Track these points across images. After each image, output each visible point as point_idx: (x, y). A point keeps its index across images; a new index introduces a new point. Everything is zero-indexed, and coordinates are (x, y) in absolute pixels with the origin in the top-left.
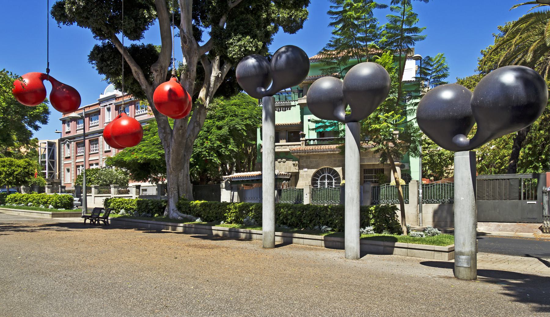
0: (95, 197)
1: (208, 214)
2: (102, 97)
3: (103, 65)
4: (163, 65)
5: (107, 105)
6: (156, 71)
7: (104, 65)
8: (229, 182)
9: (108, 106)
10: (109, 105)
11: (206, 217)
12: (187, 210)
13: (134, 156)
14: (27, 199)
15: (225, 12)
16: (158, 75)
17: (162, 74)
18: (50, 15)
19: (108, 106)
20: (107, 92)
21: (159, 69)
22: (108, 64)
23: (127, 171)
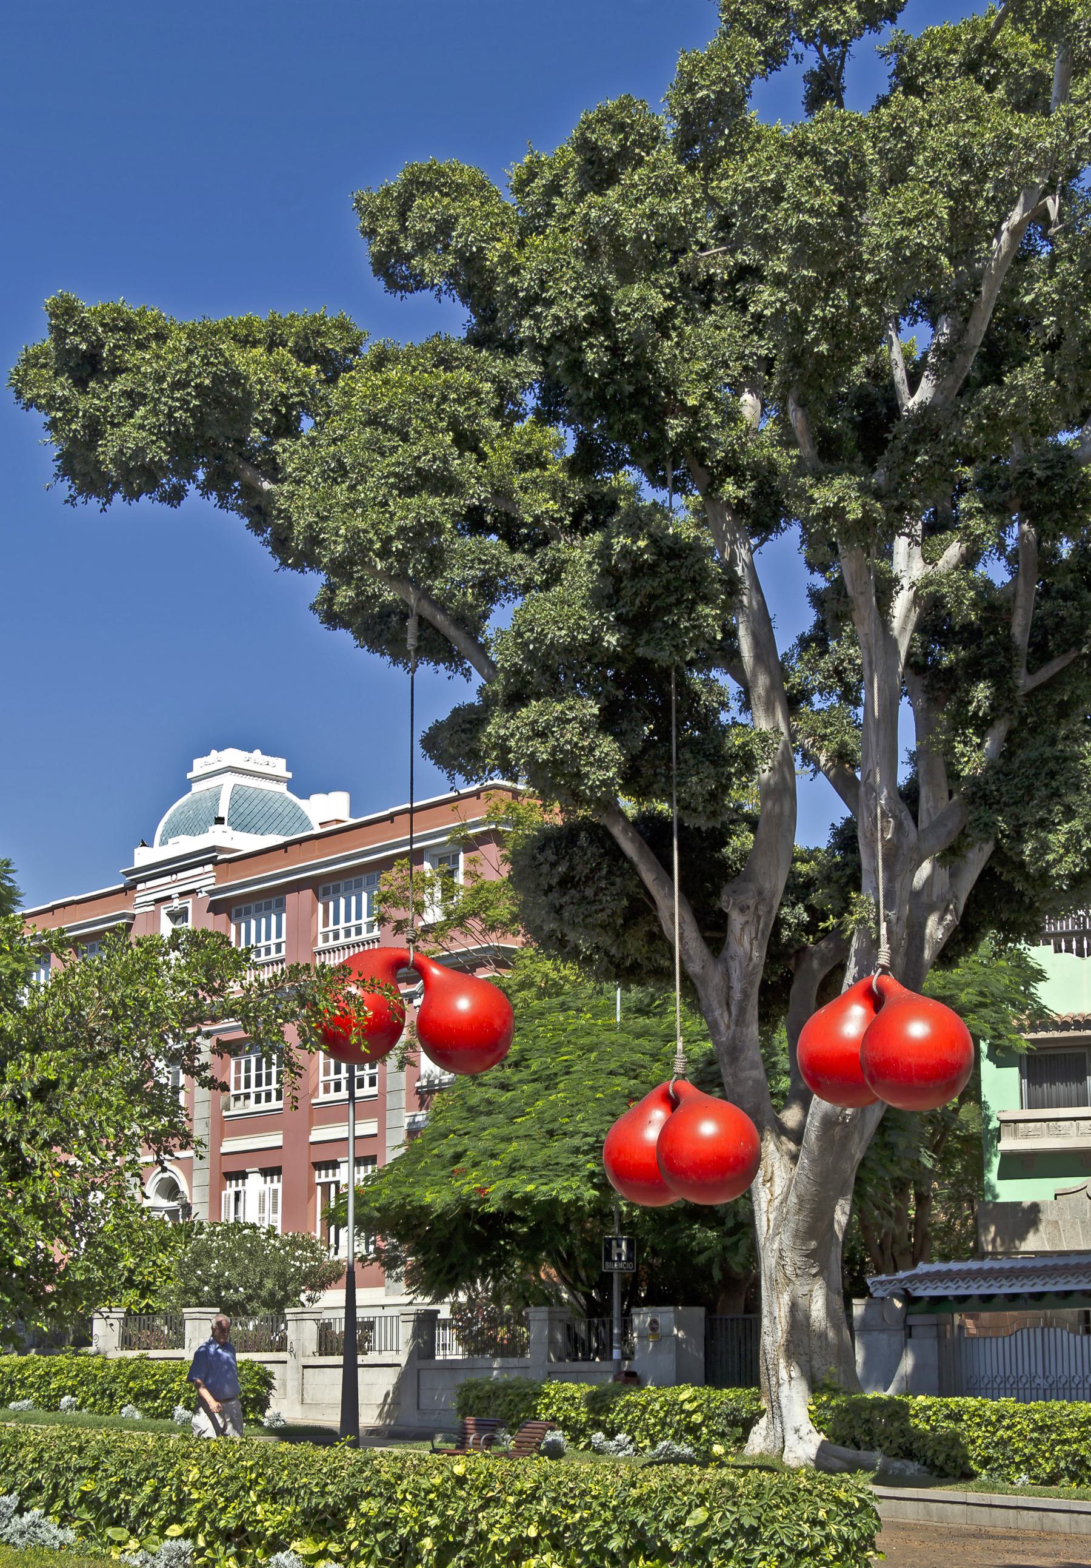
0: (305, 1367)
1: (952, 1447)
2: (143, 857)
3: (566, 898)
4: (767, 885)
5: (169, 898)
6: (743, 909)
7: (572, 898)
8: (898, 1304)
9: (176, 903)
10: (182, 895)
11: (942, 1458)
12: (857, 1432)
13: (466, 1186)
14: (46, 1378)
15: (1007, 710)
16: (747, 922)
17: (759, 918)
18: (419, 750)
19: (176, 903)
20: (173, 831)
21: (751, 903)
22: (584, 898)
23: (395, 1248)
